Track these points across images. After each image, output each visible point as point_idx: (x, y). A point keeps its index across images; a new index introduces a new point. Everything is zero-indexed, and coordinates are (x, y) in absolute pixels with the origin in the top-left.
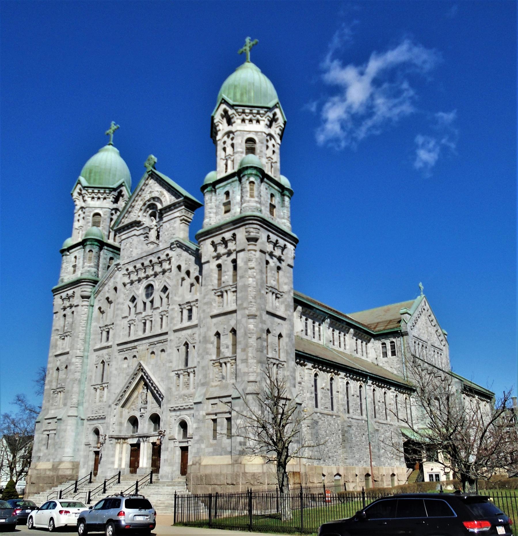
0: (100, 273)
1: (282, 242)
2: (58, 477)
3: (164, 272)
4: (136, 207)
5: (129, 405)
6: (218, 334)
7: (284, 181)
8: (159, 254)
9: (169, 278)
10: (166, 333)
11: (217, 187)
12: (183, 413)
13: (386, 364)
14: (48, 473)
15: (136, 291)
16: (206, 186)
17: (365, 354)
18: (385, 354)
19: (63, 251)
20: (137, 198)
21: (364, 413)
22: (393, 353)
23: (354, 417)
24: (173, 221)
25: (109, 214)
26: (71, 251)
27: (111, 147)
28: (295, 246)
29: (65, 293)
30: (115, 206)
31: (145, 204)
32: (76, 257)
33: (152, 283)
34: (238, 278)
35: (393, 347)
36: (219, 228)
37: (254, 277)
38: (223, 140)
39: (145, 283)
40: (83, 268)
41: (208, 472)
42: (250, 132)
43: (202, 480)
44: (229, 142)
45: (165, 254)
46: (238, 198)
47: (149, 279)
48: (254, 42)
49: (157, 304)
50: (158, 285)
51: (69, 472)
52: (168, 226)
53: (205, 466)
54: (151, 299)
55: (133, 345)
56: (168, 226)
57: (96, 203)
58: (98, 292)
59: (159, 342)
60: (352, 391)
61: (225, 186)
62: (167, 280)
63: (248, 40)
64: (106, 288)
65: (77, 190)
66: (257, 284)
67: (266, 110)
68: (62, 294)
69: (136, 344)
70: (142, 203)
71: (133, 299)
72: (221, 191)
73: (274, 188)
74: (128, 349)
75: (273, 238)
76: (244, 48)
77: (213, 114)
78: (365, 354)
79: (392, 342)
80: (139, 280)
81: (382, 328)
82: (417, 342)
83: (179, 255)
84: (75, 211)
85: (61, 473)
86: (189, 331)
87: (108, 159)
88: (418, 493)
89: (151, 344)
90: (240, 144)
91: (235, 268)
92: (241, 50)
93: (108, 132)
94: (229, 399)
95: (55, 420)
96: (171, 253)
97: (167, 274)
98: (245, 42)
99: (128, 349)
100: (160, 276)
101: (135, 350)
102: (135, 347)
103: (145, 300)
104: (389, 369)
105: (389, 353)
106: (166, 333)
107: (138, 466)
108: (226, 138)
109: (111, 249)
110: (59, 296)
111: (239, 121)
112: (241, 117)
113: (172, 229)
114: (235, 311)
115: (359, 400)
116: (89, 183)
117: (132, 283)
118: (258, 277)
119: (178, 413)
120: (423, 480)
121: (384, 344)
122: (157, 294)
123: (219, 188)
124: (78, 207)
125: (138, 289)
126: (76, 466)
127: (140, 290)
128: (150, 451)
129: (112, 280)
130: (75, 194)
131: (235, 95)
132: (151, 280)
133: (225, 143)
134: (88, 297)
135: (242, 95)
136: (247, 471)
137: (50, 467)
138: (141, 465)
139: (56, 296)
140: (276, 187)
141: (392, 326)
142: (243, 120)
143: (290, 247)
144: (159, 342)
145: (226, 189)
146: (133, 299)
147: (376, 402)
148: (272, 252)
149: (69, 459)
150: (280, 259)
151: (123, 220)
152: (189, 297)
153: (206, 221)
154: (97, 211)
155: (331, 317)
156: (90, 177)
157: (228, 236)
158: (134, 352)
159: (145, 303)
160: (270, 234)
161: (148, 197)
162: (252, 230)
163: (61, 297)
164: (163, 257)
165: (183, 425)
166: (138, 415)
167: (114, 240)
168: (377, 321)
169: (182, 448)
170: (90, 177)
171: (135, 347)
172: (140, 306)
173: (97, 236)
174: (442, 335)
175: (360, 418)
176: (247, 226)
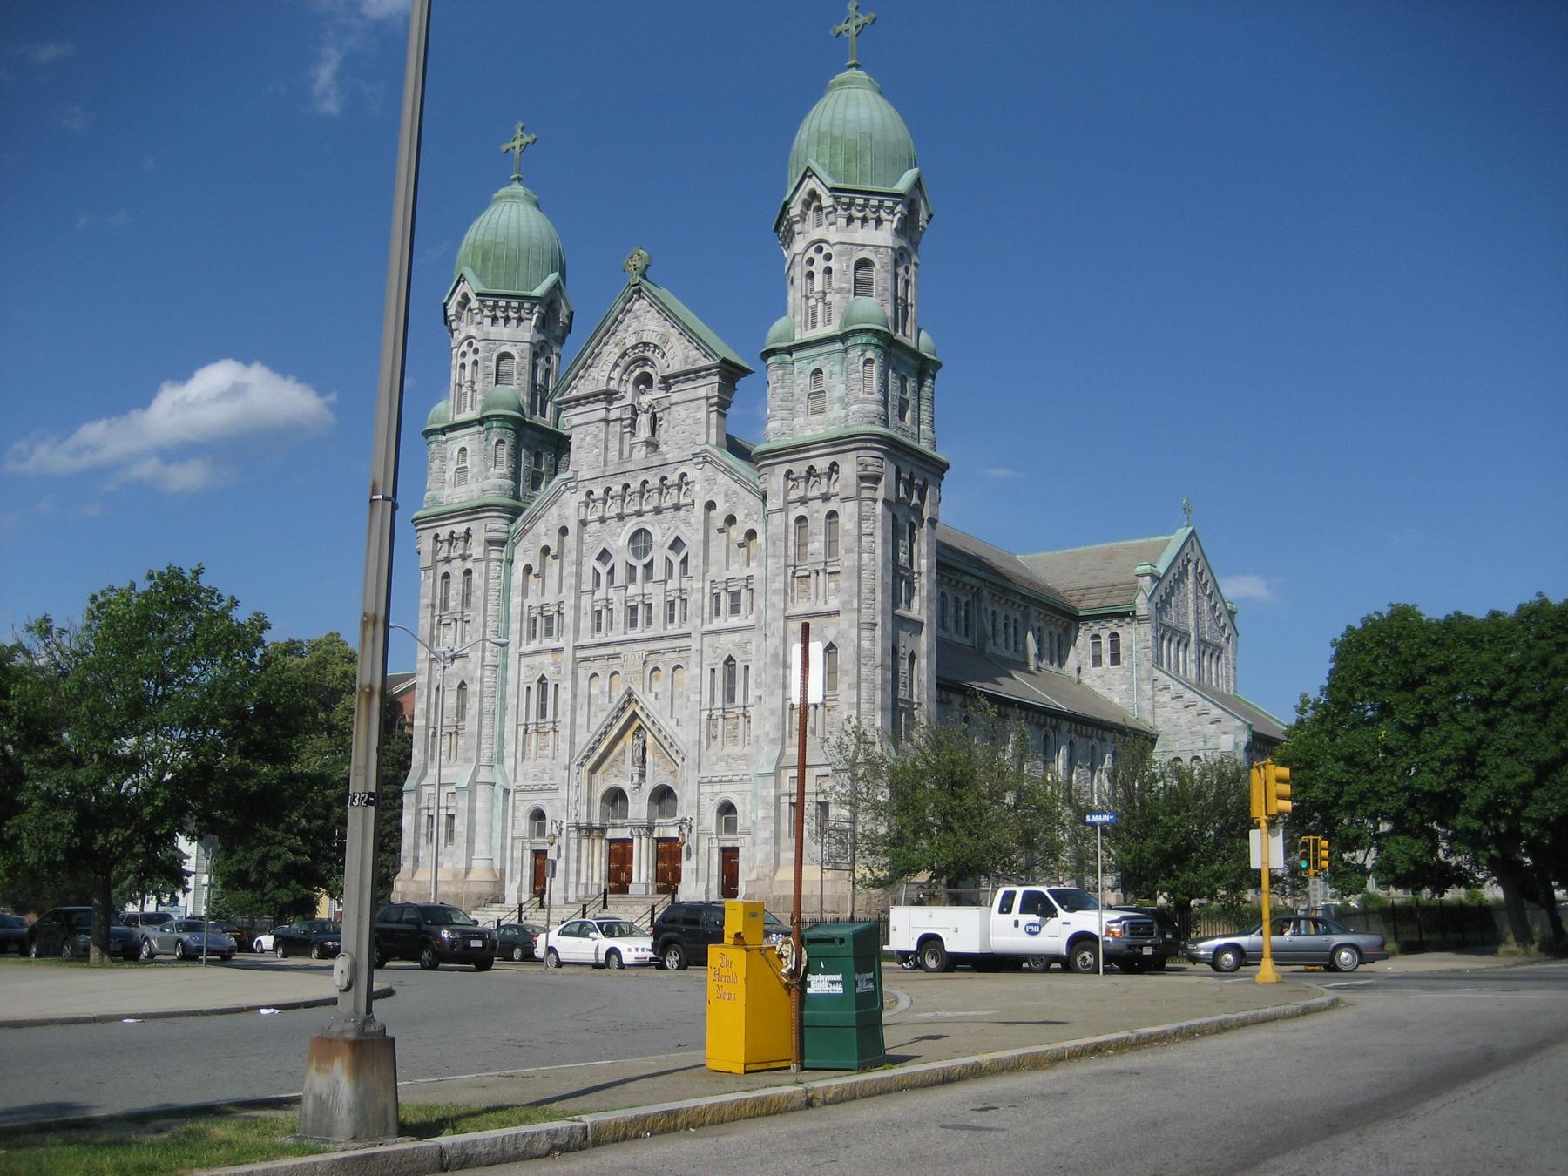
3: (677, 507)
8: (666, 471)
10: (688, 635)
12: (726, 787)
13: (1098, 682)
18: (1097, 661)
22: (1115, 659)
27: (517, 188)
31: (624, 354)
32: (463, 450)
35: (1115, 645)
39: (632, 525)
44: (820, 264)
45: (679, 472)
47: (644, 518)
49: (659, 572)
50: (661, 535)
52: (684, 414)
54: (646, 560)
55: (610, 650)
56: (684, 414)
62: (682, 527)
64: (541, 526)
68: (438, 530)
70: (617, 352)
71: (604, 556)
72: (803, 364)
74: (601, 658)
80: (620, 517)
81: (1095, 603)
83: (711, 482)
86: (736, 637)
88: (809, 433)
96: (693, 473)
97: (682, 513)
100: (669, 514)
101: (616, 661)
102: (616, 656)
105: (1106, 658)
106: (688, 635)
110: (432, 533)
113: (689, 421)
114: (837, 613)
117: (602, 520)
119: (717, 788)
121: (1097, 636)
125: (616, 536)
129: (554, 510)
132: (647, 522)
133: (811, 261)
134: (503, 543)
135: (847, 161)
141: (1116, 601)
142: (850, 220)
152: (737, 570)
153: (773, 425)
154: (505, 348)
157: (822, 465)
158: (615, 664)
159: (632, 569)
161: (631, 342)
163: (437, 536)
164: (673, 478)
165: (727, 809)
168: (1084, 584)
169: (724, 850)
171: (616, 656)
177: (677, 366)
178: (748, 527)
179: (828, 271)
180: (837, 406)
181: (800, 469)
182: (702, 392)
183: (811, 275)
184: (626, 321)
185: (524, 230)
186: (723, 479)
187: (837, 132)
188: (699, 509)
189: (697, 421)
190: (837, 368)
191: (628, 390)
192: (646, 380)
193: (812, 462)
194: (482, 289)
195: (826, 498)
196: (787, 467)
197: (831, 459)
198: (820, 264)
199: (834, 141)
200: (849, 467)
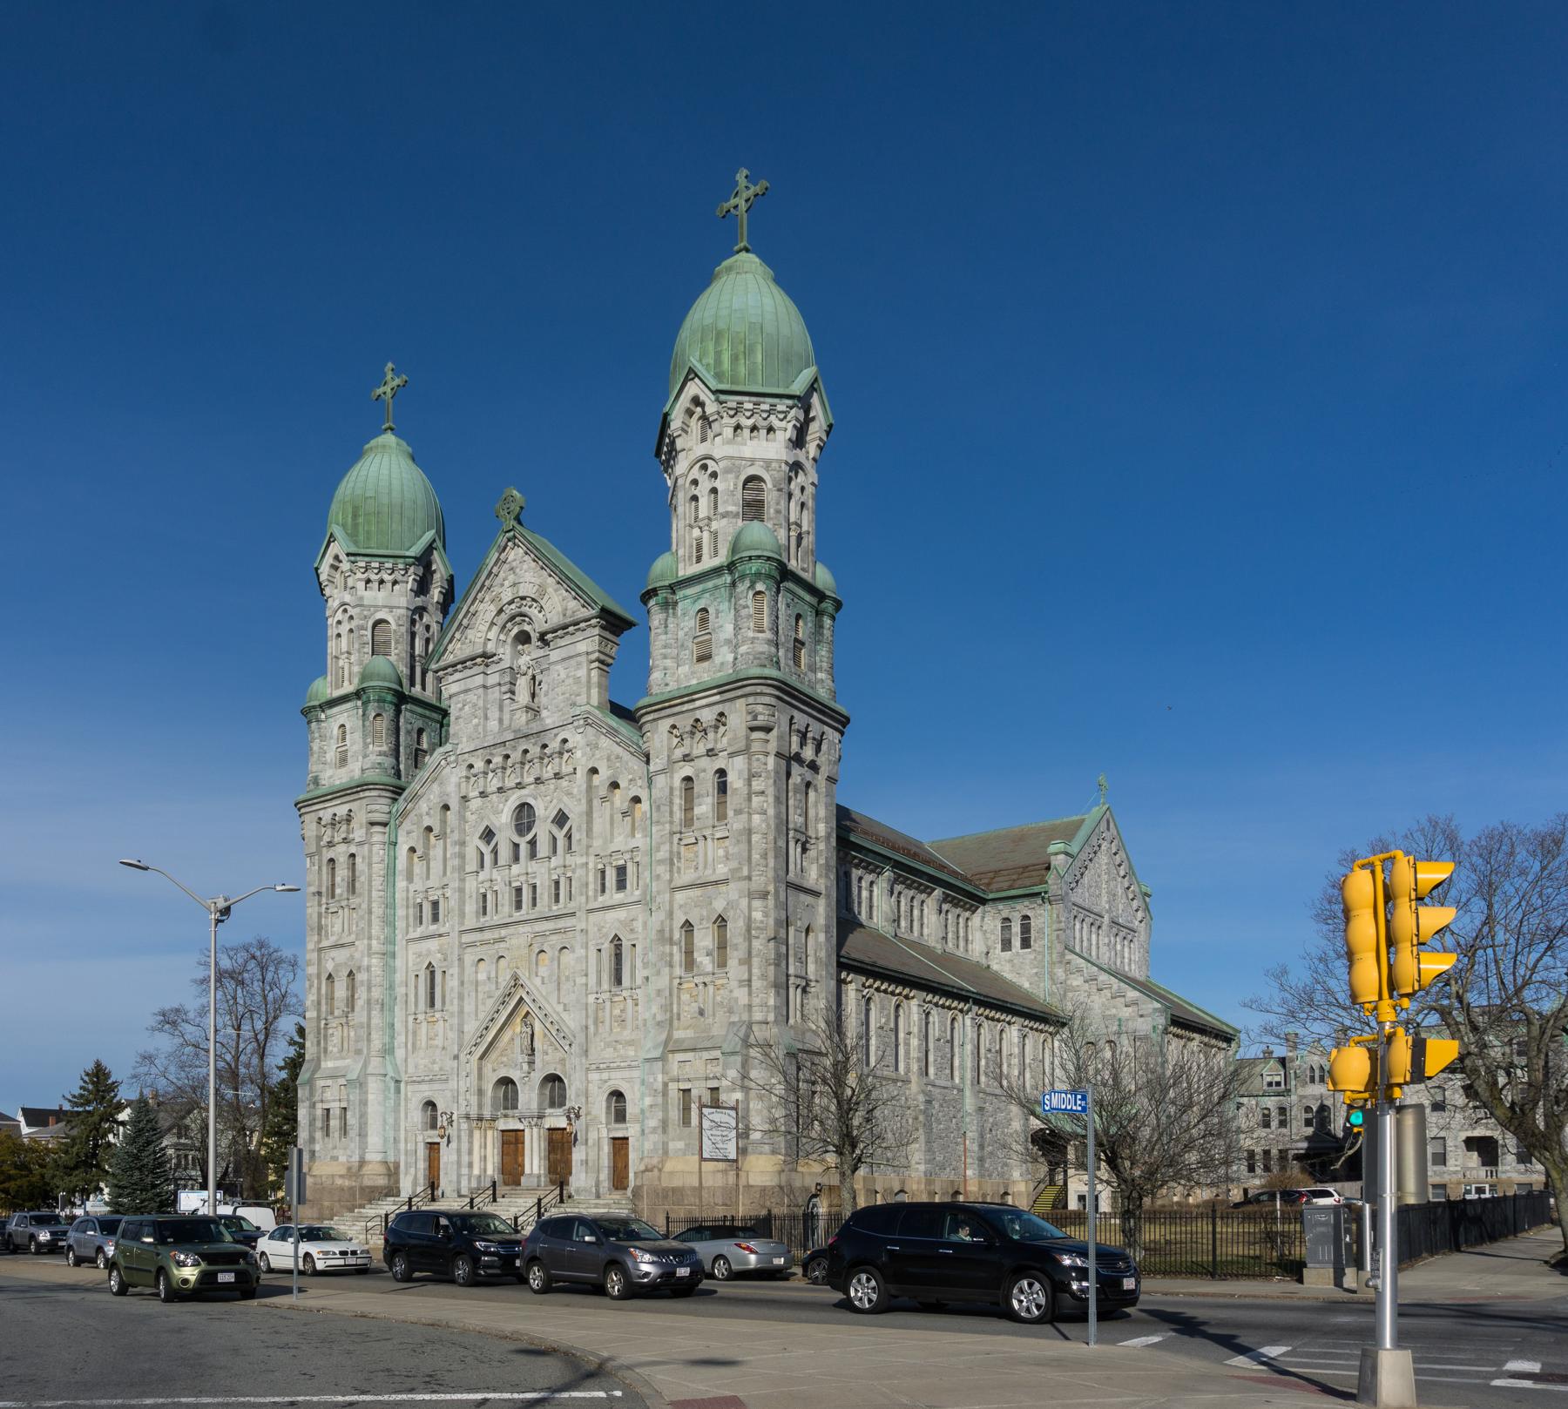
0: (402, 767)
1: (815, 728)
2: (362, 1189)
4: (480, 615)
5: (493, 1055)
6: (688, 926)
7: (823, 577)
9: (569, 794)
11: (680, 594)
14: (339, 1182)
15: (492, 817)
16: (652, 593)
17: (962, 944)
18: (1007, 945)
19: (306, 712)
20: (509, 625)
21: (956, 1073)
22: (1026, 943)
23: (938, 1082)
24: (573, 662)
25: (405, 622)
26: (329, 712)
28: (842, 734)
29: (330, 811)
30: (419, 601)
31: (501, 611)
33: (531, 801)
34: (730, 813)
35: (1026, 929)
36: (689, 696)
37: (764, 813)
38: (690, 478)
39: (514, 799)
40: (365, 756)
41: (677, 1183)
42: (752, 461)
43: (665, 1197)
45: (560, 738)
46: (729, 628)
48: (758, 189)
49: (543, 848)
50: (544, 811)
51: (382, 1181)
53: (671, 1173)
55: (496, 934)
57: (374, 596)
58: (404, 814)
59: (556, 932)
60: (934, 1032)
61: (698, 597)
63: (741, 177)
64: (423, 806)
65: (329, 559)
66: (768, 826)
67: (790, 402)
68: (321, 814)
69: (503, 932)
73: (802, 599)
74: (485, 943)
75: (801, 720)
76: (733, 202)
77: (666, 409)
78: (962, 944)
79: (1026, 917)
82: (1081, 916)
84: (328, 613)
85: (367, 1182)
87: (385, 471)
89: (537, 935)
90: (732, 493)
91: (723, 788)
92: (726, 206)
93: (380, 391)
94: (717, 1053)
95: (342, 1081)
98: (736, 183)
99: (485, 943)
101: (502, 945)
102: (502, 940)
103: (517, 839)
104: (1008, 976)
105: (1016, 942)
107: (522, 1173)
108: (696, 473)
109: (419, 710)
110: (314, 817)
111: (728, 432)
112: (733, 421)
113: (571, 681)
115: (948, 1050)
116: (356, 543)
118: (771, 812)
120: (1065, 1206)
122: (543, 829)
123: (686, 597)
124: (333, 604)
125: (499, 813)
126: (393, 1172)
127: (503, 818)
128: (544, 1145)
130: (325, 571)
131: (718, 361)
133: (695, 482)
135: (735, 359)
136: (751, 1182)
137: (343, 1172)
138: (527, 1170)
139: (307, 818)
140: (808, 597)
143: (832, 735)
144: (556, 932)
145: (701, 604)
146: (488, 835)
147: (982, 1051)
148: (797, 755)
149: (379, 1157)
150: (813, 766)
151: (450, 648)
153: (656, 676)
154: (379, 616)
155: (897, 865)
156: (355, 526)
157: (707, 716)
159: (516, 846)
160: (796, 713)
162: (760, 708)
166: (515, 1075)
167: (424, 688)
168: (994, 866)
170: (355, 526)
171: (502, 940)
172: (505, 853)
173: (384, 680)
174: (1140, 896)
175: (949, 1084)
176: (751, 700)
177: (555, 619)
178: (632, 794)
179: (714, 491)
180: (725, 649)
181: (685, 723)
182: (582, 647)
183: (695, 498)
184: (502, 574)
185: (396, 483)
186: (605, 742)
187: (722, 325)
188: (581, 774)
189: (577, 680)
190: (724, 606)
191: (505, 653)
192: (523, 638)
193: (698, 714)
194: (353, 550)
195: (711, 753)
196: (670, 721)
197: (719, 708)
198: (703, 490)
199: (719, 336)
200: (738, 716)
